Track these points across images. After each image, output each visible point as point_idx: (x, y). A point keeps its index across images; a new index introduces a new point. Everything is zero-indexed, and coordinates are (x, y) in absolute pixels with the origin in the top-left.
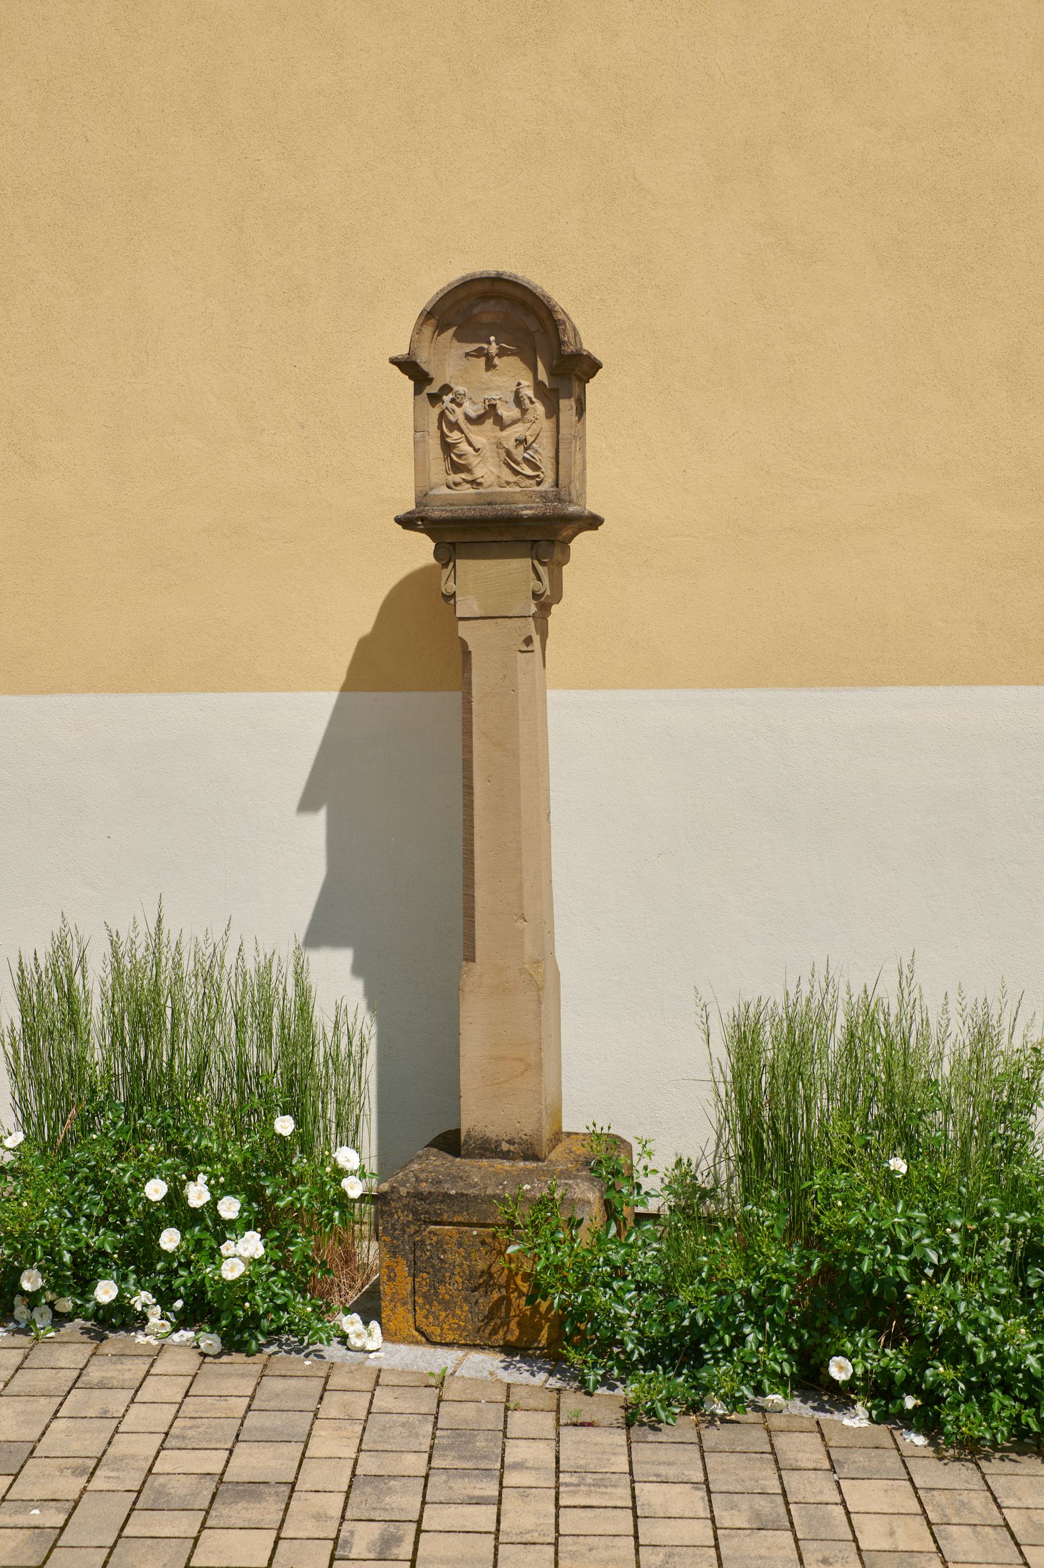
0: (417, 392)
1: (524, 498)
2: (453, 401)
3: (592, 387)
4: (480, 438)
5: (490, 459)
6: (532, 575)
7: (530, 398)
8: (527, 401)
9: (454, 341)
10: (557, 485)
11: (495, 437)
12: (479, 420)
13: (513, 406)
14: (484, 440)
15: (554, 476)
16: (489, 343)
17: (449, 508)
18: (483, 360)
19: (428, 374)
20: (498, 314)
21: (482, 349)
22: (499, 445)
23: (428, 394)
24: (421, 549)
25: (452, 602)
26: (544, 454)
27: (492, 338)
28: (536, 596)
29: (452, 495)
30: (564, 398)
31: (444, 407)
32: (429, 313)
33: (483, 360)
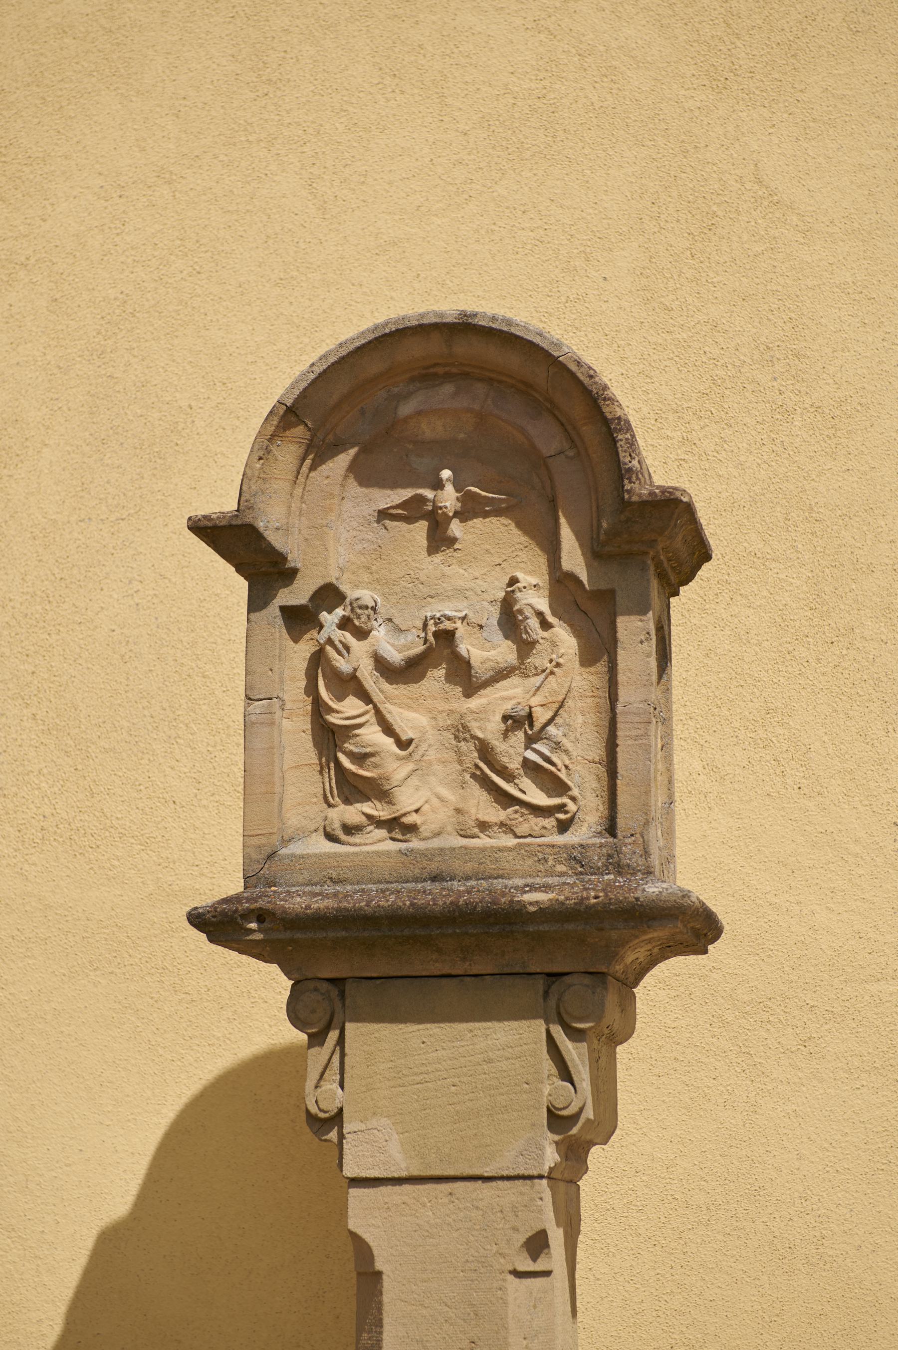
0: (256, 603)
1: (529, 864)
2: (345, 624)
3: (686, 605)
6: (548, 1065)
7: (540, 614)
8: (533, 623)
9: (352, 482)
10: (611, 828)
11: (451, 712)
13: (497, 636)
14: (423, 720)
15: (603, 809)
16: (438, 485)
17: (330, 889)
18: (422, 526)
19: (283, 558)
20: (468, 413)
21: (422, 499)
22: (461, 731)
23: (284, 609)
24: (253, 1004)
25: (333, 1135)
26: (576, 749)
27: (446, 474)
28: (557, 1120)
29: (338, 858)
30: (629, 612)
31: (323, 637)
32: (290, 410)
33: (422, 526)
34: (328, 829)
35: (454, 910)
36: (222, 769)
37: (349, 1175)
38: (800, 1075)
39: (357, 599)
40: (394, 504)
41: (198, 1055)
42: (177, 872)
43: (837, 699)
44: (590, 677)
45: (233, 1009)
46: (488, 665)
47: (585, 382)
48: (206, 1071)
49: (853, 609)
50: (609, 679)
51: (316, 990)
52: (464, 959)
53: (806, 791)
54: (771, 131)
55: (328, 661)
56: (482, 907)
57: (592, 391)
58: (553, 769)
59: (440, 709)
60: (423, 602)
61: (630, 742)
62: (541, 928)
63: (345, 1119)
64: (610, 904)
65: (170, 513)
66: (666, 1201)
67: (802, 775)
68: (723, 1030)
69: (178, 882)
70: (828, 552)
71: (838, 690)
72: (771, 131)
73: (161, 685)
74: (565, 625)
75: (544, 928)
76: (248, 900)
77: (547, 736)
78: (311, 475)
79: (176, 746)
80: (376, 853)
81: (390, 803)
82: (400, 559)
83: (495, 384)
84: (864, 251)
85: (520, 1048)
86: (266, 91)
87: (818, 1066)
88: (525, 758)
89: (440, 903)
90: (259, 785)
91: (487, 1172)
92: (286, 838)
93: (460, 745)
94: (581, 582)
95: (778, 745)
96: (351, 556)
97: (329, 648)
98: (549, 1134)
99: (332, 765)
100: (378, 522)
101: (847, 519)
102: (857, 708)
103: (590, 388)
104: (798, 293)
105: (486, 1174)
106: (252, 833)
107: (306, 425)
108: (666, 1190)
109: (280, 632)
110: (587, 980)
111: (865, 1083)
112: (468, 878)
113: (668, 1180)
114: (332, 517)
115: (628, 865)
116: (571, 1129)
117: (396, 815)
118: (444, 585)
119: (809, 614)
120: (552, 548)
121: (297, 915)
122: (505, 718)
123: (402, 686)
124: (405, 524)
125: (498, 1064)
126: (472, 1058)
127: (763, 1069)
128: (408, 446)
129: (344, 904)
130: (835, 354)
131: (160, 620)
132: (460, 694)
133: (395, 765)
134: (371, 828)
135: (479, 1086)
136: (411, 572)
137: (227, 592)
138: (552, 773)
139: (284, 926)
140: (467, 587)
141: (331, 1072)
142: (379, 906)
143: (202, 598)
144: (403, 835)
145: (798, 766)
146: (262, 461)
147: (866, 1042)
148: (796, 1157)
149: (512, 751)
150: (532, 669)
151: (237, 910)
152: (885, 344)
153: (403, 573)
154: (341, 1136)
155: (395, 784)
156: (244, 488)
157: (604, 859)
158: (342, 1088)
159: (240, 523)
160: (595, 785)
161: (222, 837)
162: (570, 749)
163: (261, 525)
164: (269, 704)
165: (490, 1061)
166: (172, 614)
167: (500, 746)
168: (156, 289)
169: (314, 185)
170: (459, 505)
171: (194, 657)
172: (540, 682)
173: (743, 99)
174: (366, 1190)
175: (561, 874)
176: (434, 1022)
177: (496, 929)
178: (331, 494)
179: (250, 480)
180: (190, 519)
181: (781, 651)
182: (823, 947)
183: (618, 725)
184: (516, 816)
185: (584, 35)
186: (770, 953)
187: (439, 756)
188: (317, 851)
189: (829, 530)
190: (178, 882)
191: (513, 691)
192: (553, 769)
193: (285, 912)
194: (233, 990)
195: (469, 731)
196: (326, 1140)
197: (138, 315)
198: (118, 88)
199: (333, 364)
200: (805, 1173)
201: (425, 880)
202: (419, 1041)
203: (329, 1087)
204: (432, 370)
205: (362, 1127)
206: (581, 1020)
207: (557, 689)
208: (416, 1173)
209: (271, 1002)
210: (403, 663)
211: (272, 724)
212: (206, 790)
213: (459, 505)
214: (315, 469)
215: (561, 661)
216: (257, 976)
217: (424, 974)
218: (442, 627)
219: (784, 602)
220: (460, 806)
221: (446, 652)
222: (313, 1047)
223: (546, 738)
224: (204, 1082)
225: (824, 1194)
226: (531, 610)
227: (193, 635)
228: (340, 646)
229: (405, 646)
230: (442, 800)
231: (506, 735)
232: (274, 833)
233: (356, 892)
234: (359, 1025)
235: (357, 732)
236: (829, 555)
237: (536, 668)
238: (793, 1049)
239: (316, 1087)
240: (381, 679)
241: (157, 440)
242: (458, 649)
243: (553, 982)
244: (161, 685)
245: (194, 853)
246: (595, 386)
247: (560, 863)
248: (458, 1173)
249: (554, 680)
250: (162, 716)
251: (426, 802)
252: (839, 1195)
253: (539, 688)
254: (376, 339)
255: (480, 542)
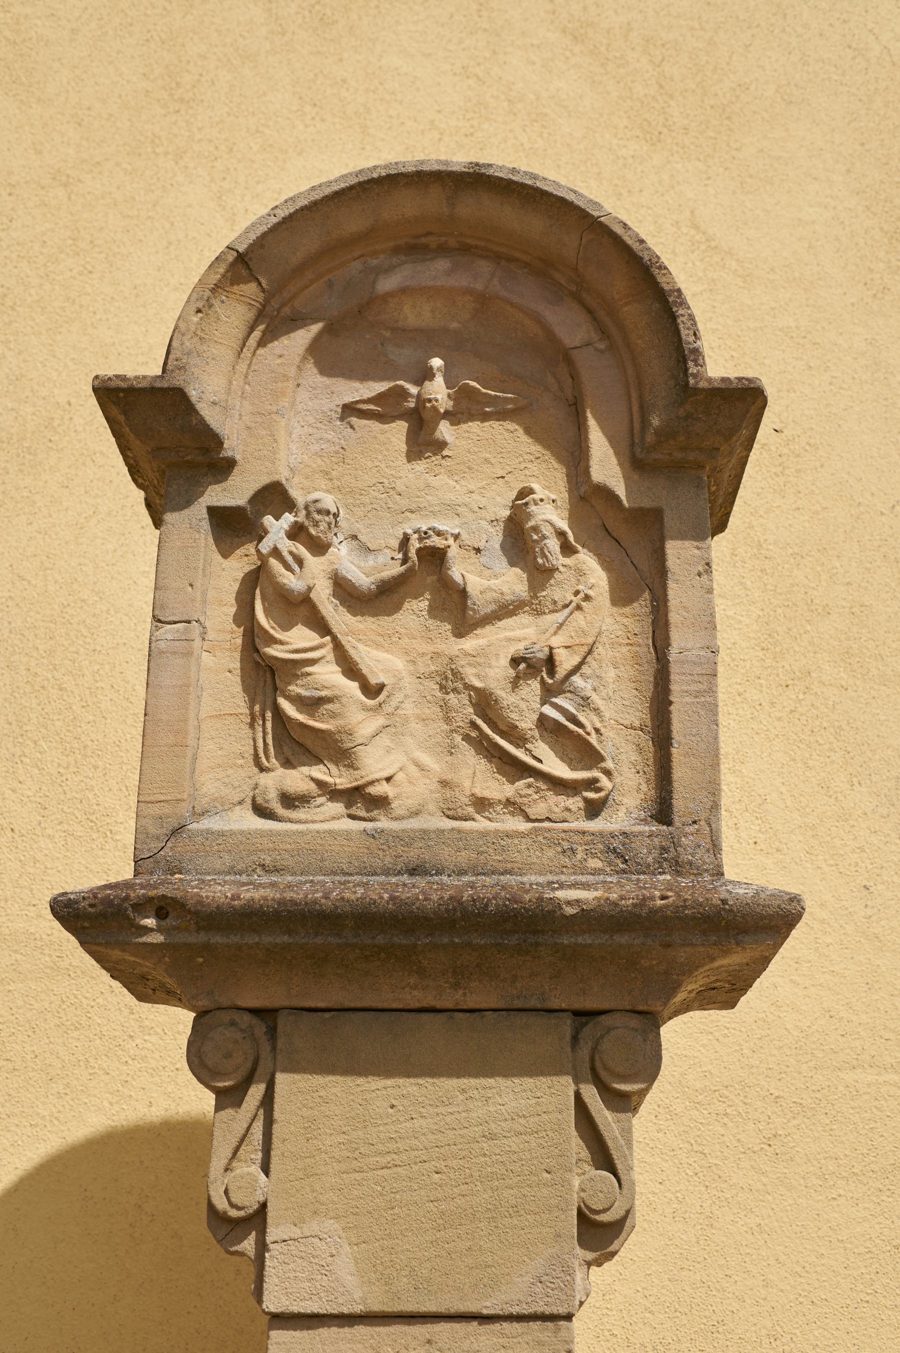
1: (555, 855)
2: (296, 532)
4: (382, 655)
5: (415, 726)
6: (577, 1146)
7: (561, 534)
8: (553, 544)
9: (311, 369)
10: (662, 811)
11: (436, 655)
12: (381, 599)
13: (501, 563)
14: (398, 663)
18: (400, 428)
19: (217, 441)
22: (450, 679)
23: (213, 511)
25: (248, 1245)
26: (611, 706)
27: (437, 362)
30: (682, 537)
33: (400, 428)
34: (259, 800)
35: (454, 909)
36: (74, 794)
37: (273, 1309)
38: (764, 1180)
39: (316, 501)
40: (365, 397)
41: (16, 1138)
42: (9, 911)
43: (795, 747)
44: (625, 620)
45: (65, 1082)
46: (489, 596)
47: (634, 247)
48: (24, 1159)
49: (809, 652)
50: (653, 621)
51: (233, 1023)
52: (456, 986)
53: (763, 846)
54: (706, 182)
55: (271, 577)
56: (497, 905)
57: (642, 258)
58: (580, 731)
59: (421, 651)
60: (400, 518)
61: (688, 699)
62: (580, 940)
63: (269, 1221)
64: (686, 907)
65: (37, 510)
66: (602, 1337)
67: (758, 828)
68: (670, 1123)
69: (10, 924)
70: (779, 590)
71: (795, 737)
72: (706, 182)
73: (8, 696)
74: (591, 554)
75: (586, 939)
76: (142, 886)
77: (572, 688)
78: (258, 352)
79: (20, 766)
80: (330, 832)
81: (352, 766)
82: (370, 464)
83: (503, 263)
84: (807, 299)
85: (537, 1119)
86: (177, 109)
87: (785, 1171)
88: (541, 714)
89: (435, 897)
90: (163, 732)
91: (488, 1307)
92: (198, 809)
93: (447, 697)
94: (616, 498)
95: (730, 794)
96: (305, 456)
97: (273, 562)
98: (578, 1250)
99: (269, 715)
100: (342, 419)
101: (799, 558)
102: (818, 758)
103: (640, 254)
104: (740, 333)
105: (485, 1312)
106: (152, 798)
107: (260, 284)
108: (602, 1324)
109: (206, 539)
110: (634, 1022)
111: (842, 1192)
112: (462, 872)
113: (605, 1311)
114: (285, 402)
115: (690, 863)
116: (612, 1243)
117: (359, 783)
118: (429, 498)
119: (760, 654)
120: (575, 459)
121: (218, 907)
122: (515, 661)
123: (370, 619)
124: (377, 424)
125: (505, 1141)
126: (465, 1131)
127: (719, 1172)
128: (384, 333)
129: (289, 895)
130: (781, 394)
131: (13, 625)
132: (449, 633)
133: (361, 716)
134: (322, 800)
135: (476, 1174)
136: (385, 480)
137: (95, 598)
138: (579, 735)
139: (197, 923)
140: (460, 501)
141: (249, 1148)
142: (343, 898)
143: (65, 603)
144: (367, 812)
145: (753, 819)
146: (200, 315)
147: (842, 1142)
148: (761, 1283)
149: (523, 705)
150: (548, 603)
151: (127, 898)
152: (832, 387)
153: (374, 481)
154: (262, 1247)
155: (360, 741)
156: (174, 344)
157: (655, 853)
158: (267, 1174)
159: (166, 386)
160: (634, 757)
161: (68, 872)
162: (602, 708)
163: (193, 395)
164: (186, 629)
165: (492, 1137)
166: (28, 619)
167: (506, 697)
168: (41, 285)
169: (224, 198)
170: (451, 403)
171: (51, 667)
172: (563, 618)
173: (677, 152)
174: (297, 1334)
175: (596, 872)
176: (409, 1076)
177: (514, 940)
178: (285, 376)
179: (183, 335)
180: (97, 377)
181: (730, 693)
182: (788, 1027)
183: (672, 677)
184: (530, 791)
185: (513, 84)
186: (726, 1031)
187: (419, 712)
188: (245, 828)
189: (780, 568)
190: (10, 924)
191: (522, 631)
192: (580, 731)
193: (200, 902)
194: (67, 1058)
195: (462, 679)
196: (236, 1253)
197: (18, 309)
198: (17, 94)
199: (302, 209)
200: (774, 1304)
201: (399, 873)
202: (386, 1104)
203: (246, 1170)
204: (424, 240)
205: (296, 1232)
206: (625, 1079)
207: (586, 629)
208: (376, 1307)
209: (114, 1074)
210: (373, 587)
211: (189, 654)
212: (52, 818)
213: (451, 403)
214: (264, 346)
215: (591, 593)
216: (98, 1041)
217: (395, 1006)
218: (428, 543)
219: (733, 641)
220: (448, 777)
221: (431, 579)
222: (223, 1109)
223: (570, 691)
224: (20, 1173)
225: (798, 1332)
226: (550, 528)
227: (52, 642)
228: (289, 559)
229: (374, 568)
230: (421, 767)
231: (515, 684)
232: (184, 800)
233: (306, 882)
234: (297, 1077)
235: (308, 669)
236: (781, 594)
237: (555, 602)
238: (756, 1149)
239: (226, 1170)
240: (341, 608)
241: (29, 435)
242: (450, 572)
243: (585, 1024)
244: (8, 696)
245: (31, 890)
246: (646, 253)
247: (594, 856)
248: (442, 1309)
249: (581, 617)
250: (6, 731)
251: (401, 769)
252: (816, 1333)
253: (562, 625)
254: (360, 184)
255: (476, 450)
